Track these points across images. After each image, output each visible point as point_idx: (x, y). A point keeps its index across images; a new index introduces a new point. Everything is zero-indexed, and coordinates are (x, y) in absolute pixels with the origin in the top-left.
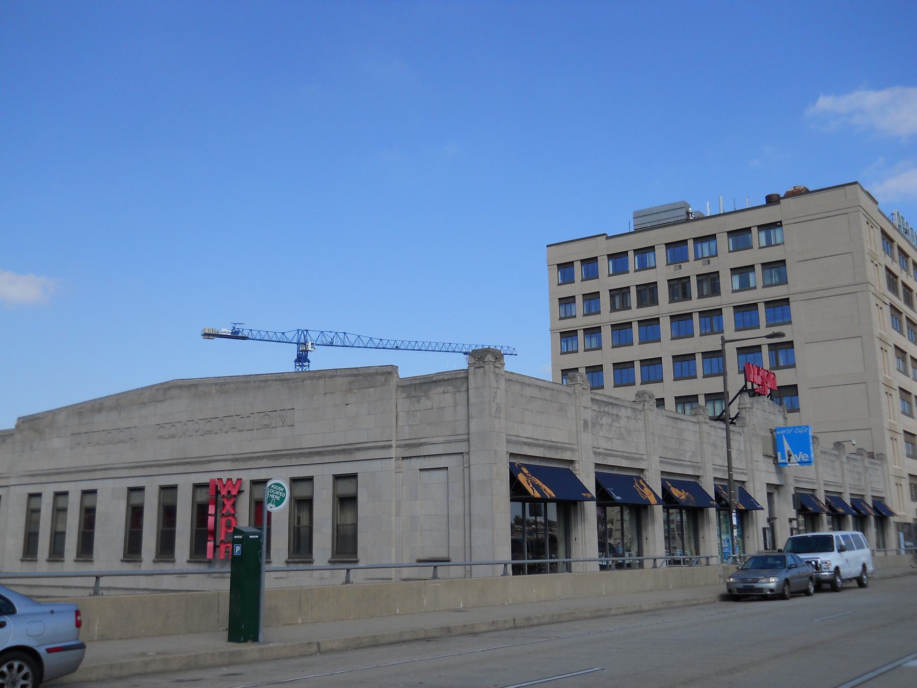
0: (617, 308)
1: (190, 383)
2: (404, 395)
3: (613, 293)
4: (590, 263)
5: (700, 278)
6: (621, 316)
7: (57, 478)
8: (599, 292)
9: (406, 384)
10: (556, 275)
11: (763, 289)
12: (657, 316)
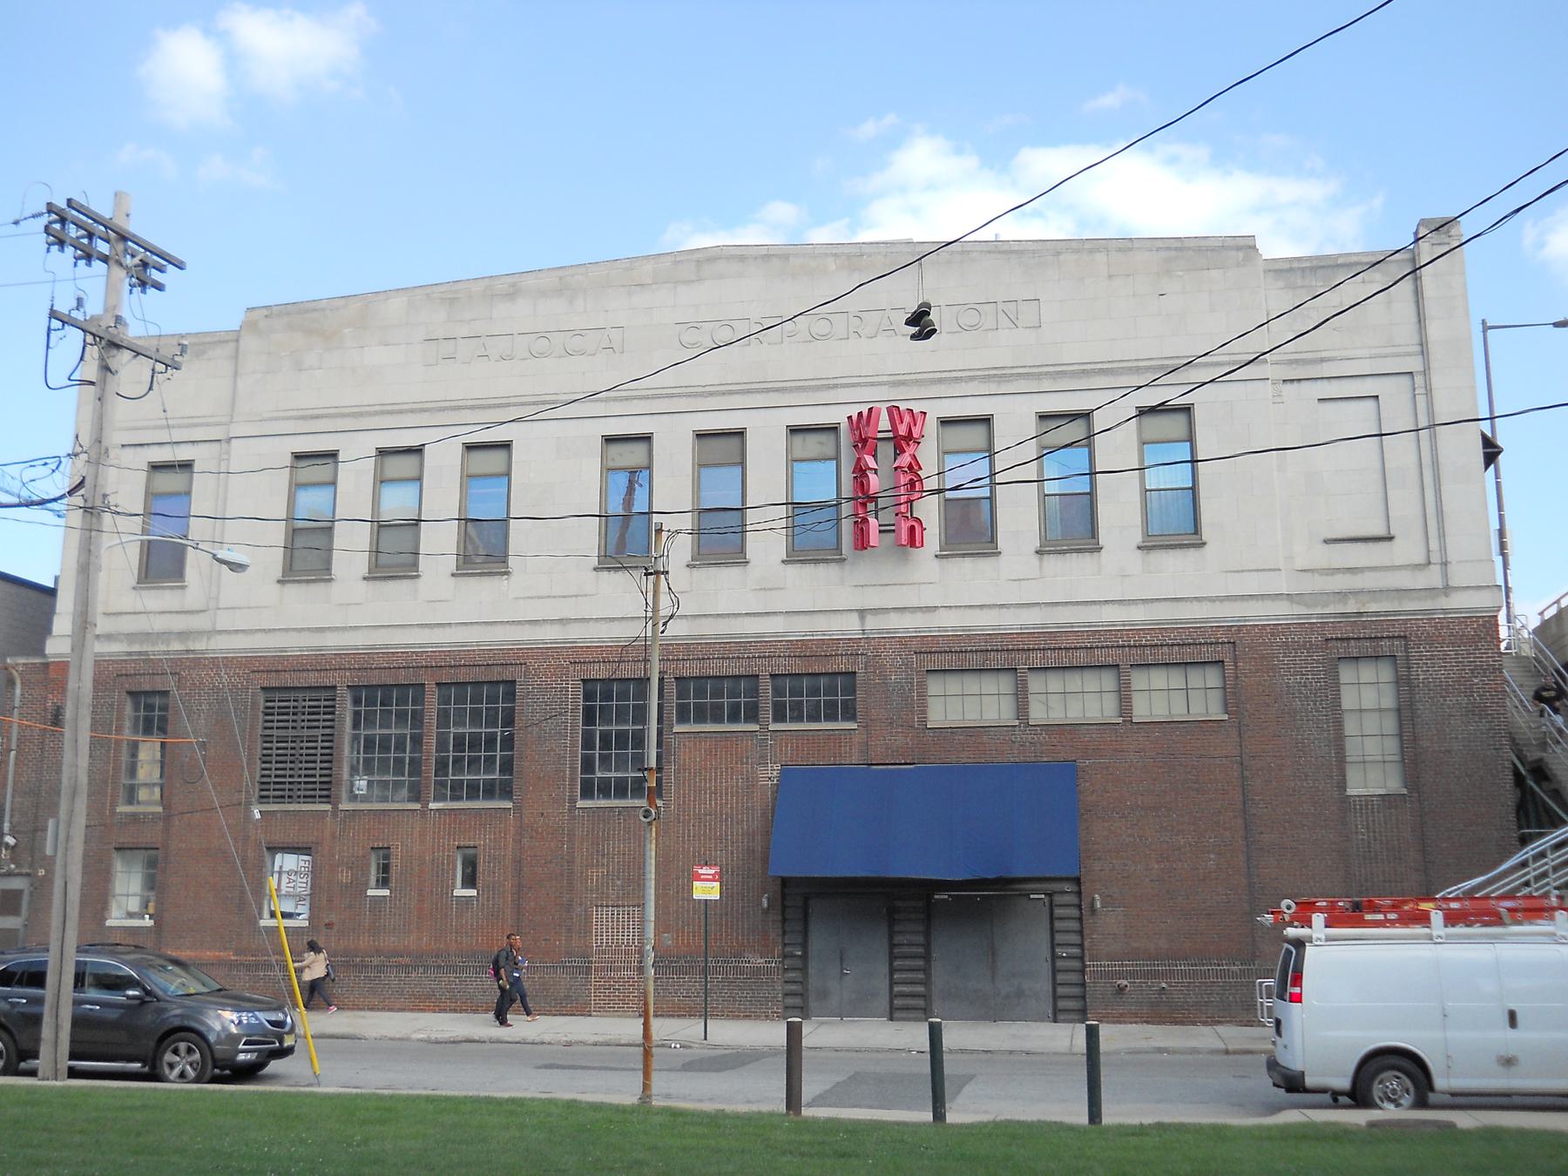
2: (1281, 284)
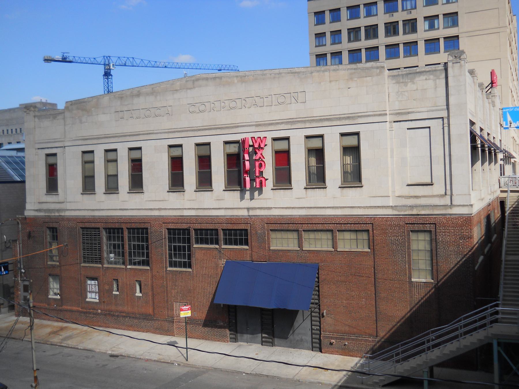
0: (352, 40)
1: (214, 76)
2: (394, 81)
3: (350, 30)
4: (335, 12)
5: (405, 22)
6: (355, 45)
7: (171, 135)
8: (341, 30)
9: (394, 74)
10: (313, 19)
11: (444, 30)
12: (378, 46)
